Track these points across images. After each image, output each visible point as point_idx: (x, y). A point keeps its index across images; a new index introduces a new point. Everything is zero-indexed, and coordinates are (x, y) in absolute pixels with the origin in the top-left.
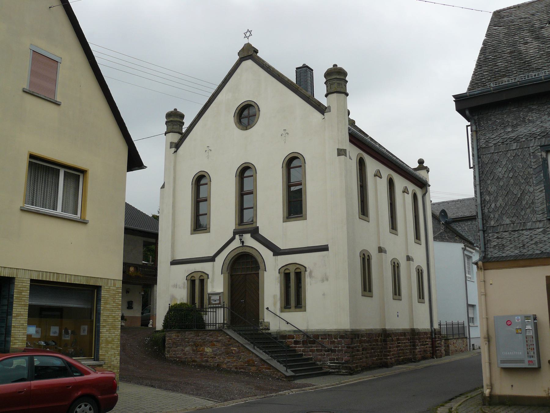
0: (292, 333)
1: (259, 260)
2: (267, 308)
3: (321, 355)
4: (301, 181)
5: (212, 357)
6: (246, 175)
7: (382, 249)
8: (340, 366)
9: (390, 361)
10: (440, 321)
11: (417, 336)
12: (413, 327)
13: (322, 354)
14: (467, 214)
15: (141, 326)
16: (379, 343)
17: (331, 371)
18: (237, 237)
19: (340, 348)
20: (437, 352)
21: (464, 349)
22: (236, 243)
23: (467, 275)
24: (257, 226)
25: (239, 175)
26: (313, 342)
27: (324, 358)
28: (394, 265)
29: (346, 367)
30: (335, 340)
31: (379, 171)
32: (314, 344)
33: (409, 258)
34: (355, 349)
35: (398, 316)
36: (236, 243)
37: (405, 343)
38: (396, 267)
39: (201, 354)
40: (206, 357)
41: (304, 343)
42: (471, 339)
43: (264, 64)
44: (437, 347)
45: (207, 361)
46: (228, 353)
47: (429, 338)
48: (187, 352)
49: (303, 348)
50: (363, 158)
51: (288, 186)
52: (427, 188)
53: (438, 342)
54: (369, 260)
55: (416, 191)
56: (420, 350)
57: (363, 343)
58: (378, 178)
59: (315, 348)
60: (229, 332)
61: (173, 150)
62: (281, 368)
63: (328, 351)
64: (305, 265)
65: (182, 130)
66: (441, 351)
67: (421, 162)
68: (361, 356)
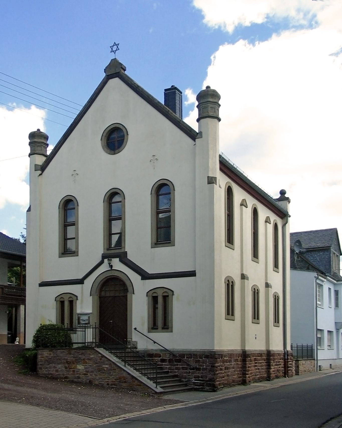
0: (158, 352)
1: (128, 283)
2: (135, 329)
3: (186, 373)
4: (121, 216)
5: (85, 374)
6: (114, 200)
7: (245, 276)
8: (204, 383)
9: (248, 379)
10: (312, 344)
11: (272, 357)
12: (269, 349)
13: (187, 372)
14: (320, 245)
15: (8, 343)
16: (239, 363)
17: (195, 387)
18: (106, 261)
19: (204, 367)
20: (289, 371)
21: (312, 370)
22: (104, 268)
23: (318, 302)
24: (126, 251)
25: (107, 201)
26: (179, 361)
27: (189, 375)
28: (254, 291)
29: (210, 384)
30: (200, 359)
31: (244, 200)
32: (180, 363)
33: (267, 285)
34: (219, 368)
35: (256, 338)
36: (104, 268)
37: (261, 363)
38: (256, 293)
39: (74, 371)
40: (78, 374)
41: (170, 361)
42: (318, 360)
43: (133, 83)
44: (288, 367)
45: (79, 378)
46: (100, 370)
47: (282, 359)
48: (59, 369)
49: (169, 366)
50: (231, 188)
51: (157, 213)
52: (287, 219)
53: (290, 363)
54: (232, 286)
55: (278, 221)
56: (274, 370)
57: (225, 362)
58: (244, 207)
59: (181, 367)
60: (101, 351)
61: (40, 172)
62: (151, 384)
63: (193, 369)
64: (172, 290)
65: (46, 152)
66: (292, 371)
67: (283, 193)
68: (223, 374)
